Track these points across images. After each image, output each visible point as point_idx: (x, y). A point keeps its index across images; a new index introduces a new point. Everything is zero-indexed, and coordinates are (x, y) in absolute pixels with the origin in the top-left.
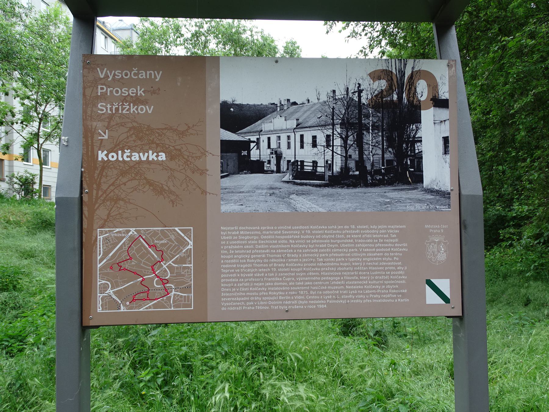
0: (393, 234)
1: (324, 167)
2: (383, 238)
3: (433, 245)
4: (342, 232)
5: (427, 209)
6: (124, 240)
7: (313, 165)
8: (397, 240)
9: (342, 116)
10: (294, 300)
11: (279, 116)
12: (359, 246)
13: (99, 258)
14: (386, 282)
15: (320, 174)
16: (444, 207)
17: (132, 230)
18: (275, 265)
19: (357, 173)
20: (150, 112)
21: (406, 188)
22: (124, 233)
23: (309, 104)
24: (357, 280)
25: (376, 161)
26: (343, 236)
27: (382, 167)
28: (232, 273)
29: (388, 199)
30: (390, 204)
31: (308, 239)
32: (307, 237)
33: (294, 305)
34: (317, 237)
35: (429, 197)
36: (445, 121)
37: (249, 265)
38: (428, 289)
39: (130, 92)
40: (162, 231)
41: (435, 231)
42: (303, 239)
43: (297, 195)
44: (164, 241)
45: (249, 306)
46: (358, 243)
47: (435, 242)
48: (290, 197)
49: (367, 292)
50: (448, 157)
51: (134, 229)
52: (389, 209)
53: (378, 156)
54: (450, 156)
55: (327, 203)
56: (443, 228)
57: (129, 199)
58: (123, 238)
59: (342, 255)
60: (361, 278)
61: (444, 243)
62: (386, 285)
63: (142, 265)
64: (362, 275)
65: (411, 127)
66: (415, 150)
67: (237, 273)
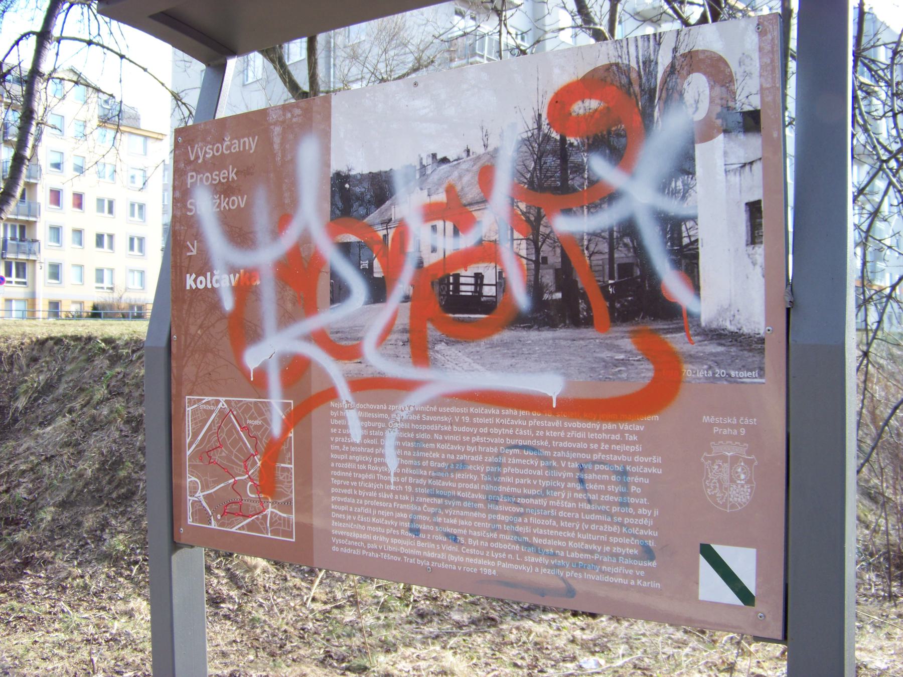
0: (631, 433)
1: (495, 285)
2: (609, 442)
3: (719, 466)
4: (527, 423)
5: (707, 378)
6: (214, 415)
7: (476, 281)
8: (638, 448)
9: (528, 176)
10: (441, 551)
11: (418, 188)
12: (559, 455)
13: (188, 441)
14: (614, 540)
15: (487, 301)
16: (749, 373)
17: (222, 399)
18: (411, 480)
19: (559, 295)
20: (242, 206)
21: (662, 327)
22: (213, 405)
23: (469, 158)
24: (554, 528)
25: (597, 268)
26: (528, 432)
27: (611, 282)
28: (347, 487)
29: (621, 353)
30: (625, 365)
31: (466, 434)
32: (464, 429)
33: (440, 561)
34: (481, 430)
35: (713, 348)
36: (751, 163)
37: (371, 476)
38: (704, 566)
39: (222, 176)
40: (255, 403)
41: (725, 432)
42: (457, 433)
43: (447, 343)
44: (258, 422)
45: (371, 550)
46: (559, 449)
47: (724, 458)
48: (436, 348)
49: (573, 555)
50: (759, 251)
51: (224, 399)
52: (624, 375)
53: (602, 257)
54: (765, 250)
55: (501, 361)
56: (744, 426)
57: (219, 350)
58: (212, 412)
59: (526, 471)
60: (562, 524)
61: (746, 461)
62: (612, 545)
63: (233, 458)
64: (564, 519)
65: (673, 185)
66: (680, 238)
67: (353, 488)
